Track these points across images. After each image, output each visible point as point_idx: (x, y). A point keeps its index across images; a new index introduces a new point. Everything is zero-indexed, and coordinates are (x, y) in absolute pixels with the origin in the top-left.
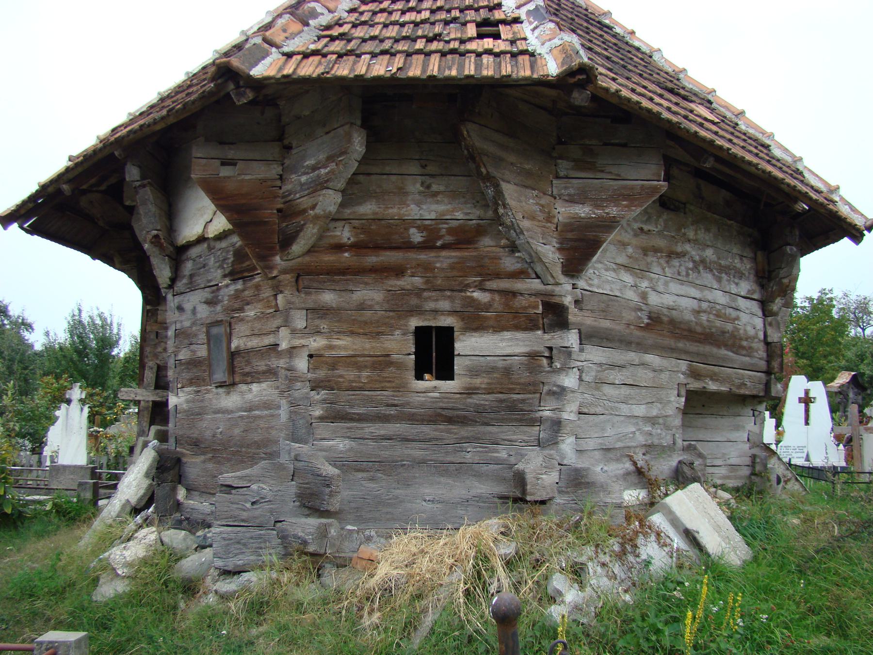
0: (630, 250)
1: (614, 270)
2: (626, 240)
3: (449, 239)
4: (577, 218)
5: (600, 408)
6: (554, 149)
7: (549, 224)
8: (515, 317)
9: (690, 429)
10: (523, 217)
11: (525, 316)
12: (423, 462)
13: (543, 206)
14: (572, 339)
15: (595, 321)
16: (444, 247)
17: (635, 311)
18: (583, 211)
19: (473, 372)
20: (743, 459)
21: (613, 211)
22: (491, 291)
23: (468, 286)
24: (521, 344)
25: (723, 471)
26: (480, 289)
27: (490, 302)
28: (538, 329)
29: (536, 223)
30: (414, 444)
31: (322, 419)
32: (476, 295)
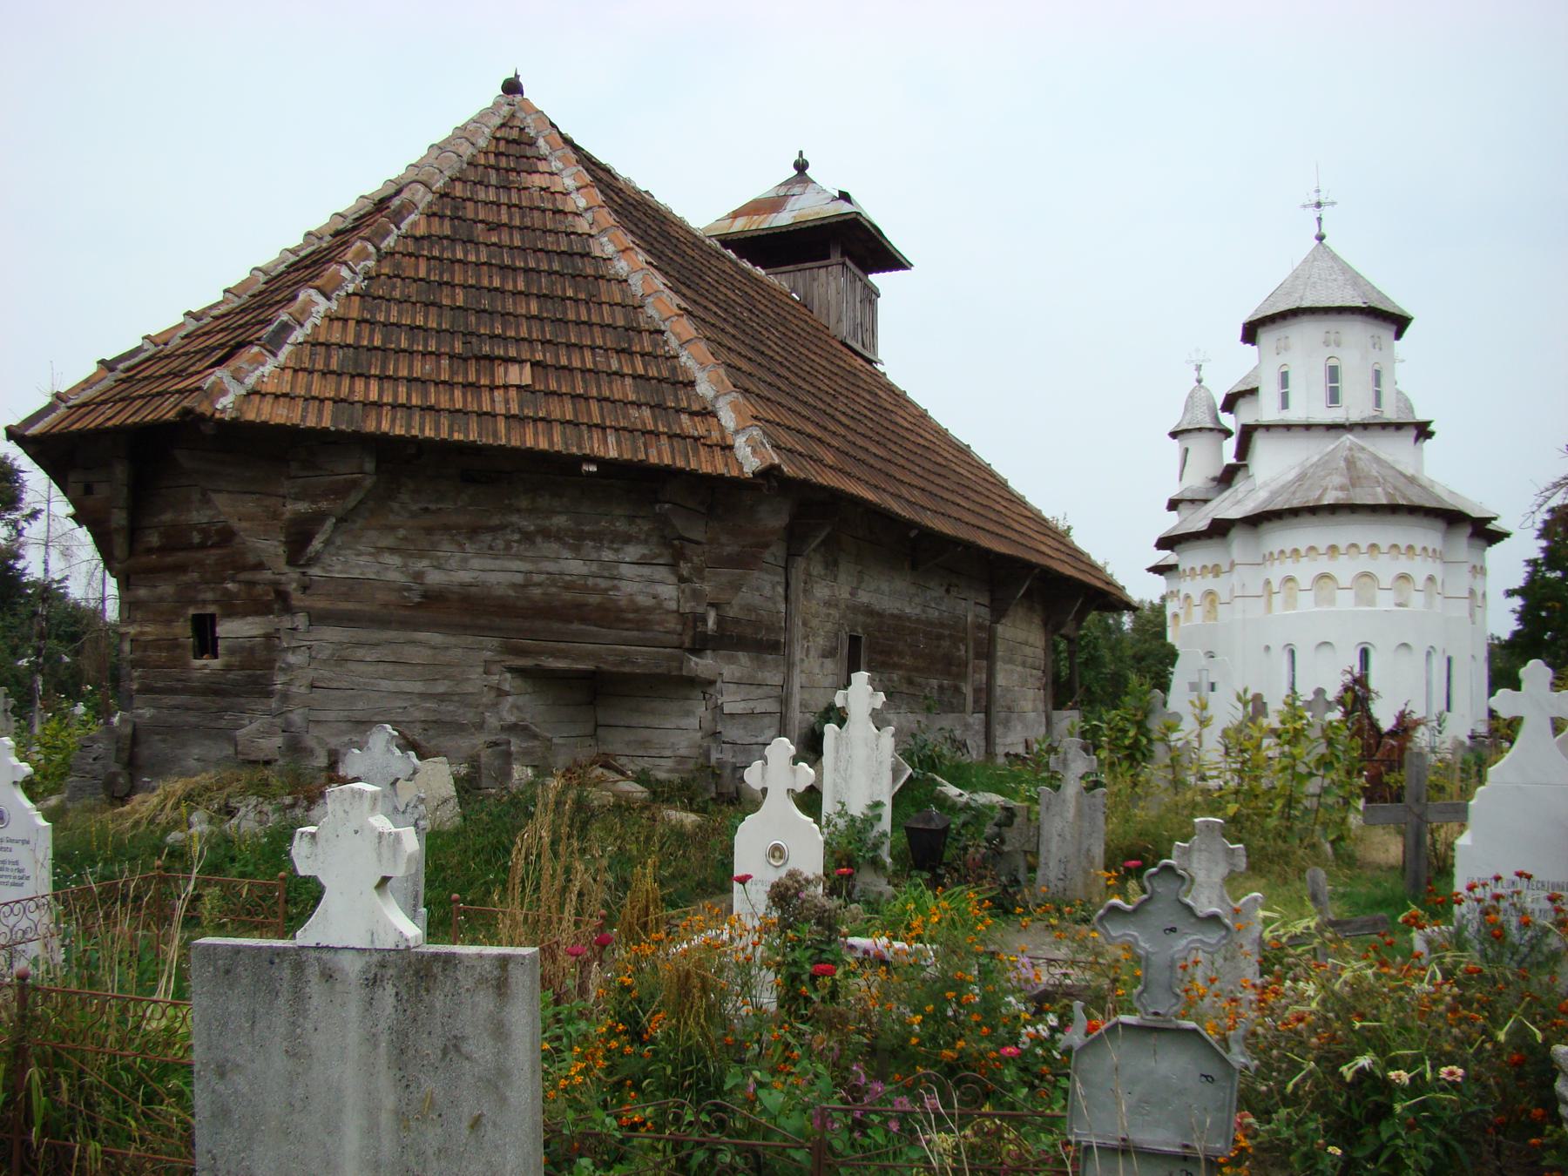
0: (401, 533)
1: (370, 554)
3: (215, 539)
12: (196, 727)
14: (301, 621)
16: (212, 546)
18: (303, 507)
19: (231, 651)
21: (324, 505)
22: (239, 582)
25: (669, 763)
28: (272, 613)
30: (191, 712)
31: (138, 691)
32: (230, 586)
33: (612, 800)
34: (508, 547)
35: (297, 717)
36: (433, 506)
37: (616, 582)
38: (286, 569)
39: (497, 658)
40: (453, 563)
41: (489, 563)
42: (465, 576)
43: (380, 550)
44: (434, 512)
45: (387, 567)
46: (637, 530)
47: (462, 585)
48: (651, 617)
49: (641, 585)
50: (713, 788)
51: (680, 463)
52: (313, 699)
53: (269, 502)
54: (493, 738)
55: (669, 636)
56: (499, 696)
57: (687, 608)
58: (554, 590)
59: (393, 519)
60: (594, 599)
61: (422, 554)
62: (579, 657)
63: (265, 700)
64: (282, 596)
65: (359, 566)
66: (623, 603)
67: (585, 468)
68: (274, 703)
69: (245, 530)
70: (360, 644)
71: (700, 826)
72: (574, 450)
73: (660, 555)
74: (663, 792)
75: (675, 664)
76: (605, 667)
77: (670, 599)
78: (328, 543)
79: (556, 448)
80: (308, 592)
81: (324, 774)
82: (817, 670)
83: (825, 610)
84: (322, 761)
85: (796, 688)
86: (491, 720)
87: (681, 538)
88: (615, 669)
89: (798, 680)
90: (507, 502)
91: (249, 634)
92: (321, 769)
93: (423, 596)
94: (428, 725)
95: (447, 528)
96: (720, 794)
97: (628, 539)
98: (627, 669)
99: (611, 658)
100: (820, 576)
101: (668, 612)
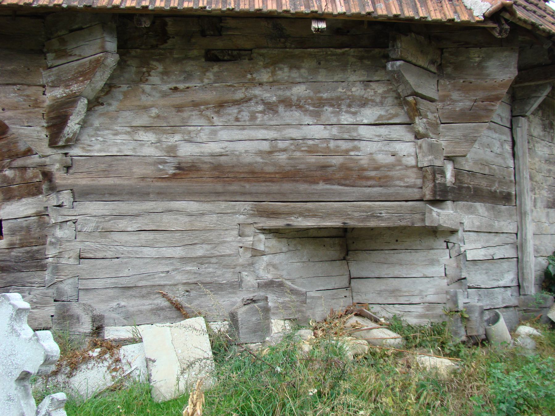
0: (154, 111)
2: (149, 103)
4: (55, 99)
5: (111, 253)
6: (44, 46)
7: (37, 109)
8: (28, 186)
9: (386, 266)
10: (3, 110)
11: (33, 185)
13: (28, 96)
14: (66, 197)
15: (93, 180)
17: (154, 165)
18: (59, 93)
19: (13, 232)
20: (441, 296)
21: (75, 88)
23: (4, 167)
24: (31, 206)
25: (419, 309)
26: (9, 168)
27: (14, 177)
28: (41, 193)
29: (21, 111)
33: (367, 348)
34: (253, 117)
35: (67, 287)
36: (181, 86)
37: (356, 143)
38: (49, 151)
39: (250, 221)
40: (203, 136)
41: (236, 134)
42: (214, 147)
43: (136, 128)
44: (182, 91)
45: (142, 144)
46: (372, 93)
47: (212, 155)
48: (391, 173)
49: (380, 144)
50: (462, 332)
51: (408, 13)
52: (81, 269)
53: (30, 91)
54: (251, 296)
55: (410, 190)
56: (253, 256)
57: (425, 162)
58: (298, 154)
59: (145, 100)
60: (336, 160)
61: (174, 129)
62: (328, 215)
63: (40, 273)
64: (48, 176)
65: (116, 144)
66: (364, 162)
67: (315, 25)
68: (47, 275)
69: (9, 118)
70: (121, 216)
71: (455, 372)
72: (302, 9)
73: (396, 115)
74: (415, 337)
75: (418, 216)
76: (352, 223)
77: (409, 155)
78: (84, 124)
79: (284, 8)
80: (71, 171)
81: (88, 339)
82: (544, 220)
83: (546, 167)
84: (86, 327)
85: (530, 235)
86: (248, 279)
87: (415, 94)
88: (361, 225)
89: (530, 228)
90: (249, 76)
91: (25, 214)
92: (86, 335)
93: (178, 168)
94: (190, 287)
95: (195, 105)
96: (469, 337)
97: (364, 103)
98: (372, 224)
99: (356, 214)
100: (539, 137)
101: (407, 167)
